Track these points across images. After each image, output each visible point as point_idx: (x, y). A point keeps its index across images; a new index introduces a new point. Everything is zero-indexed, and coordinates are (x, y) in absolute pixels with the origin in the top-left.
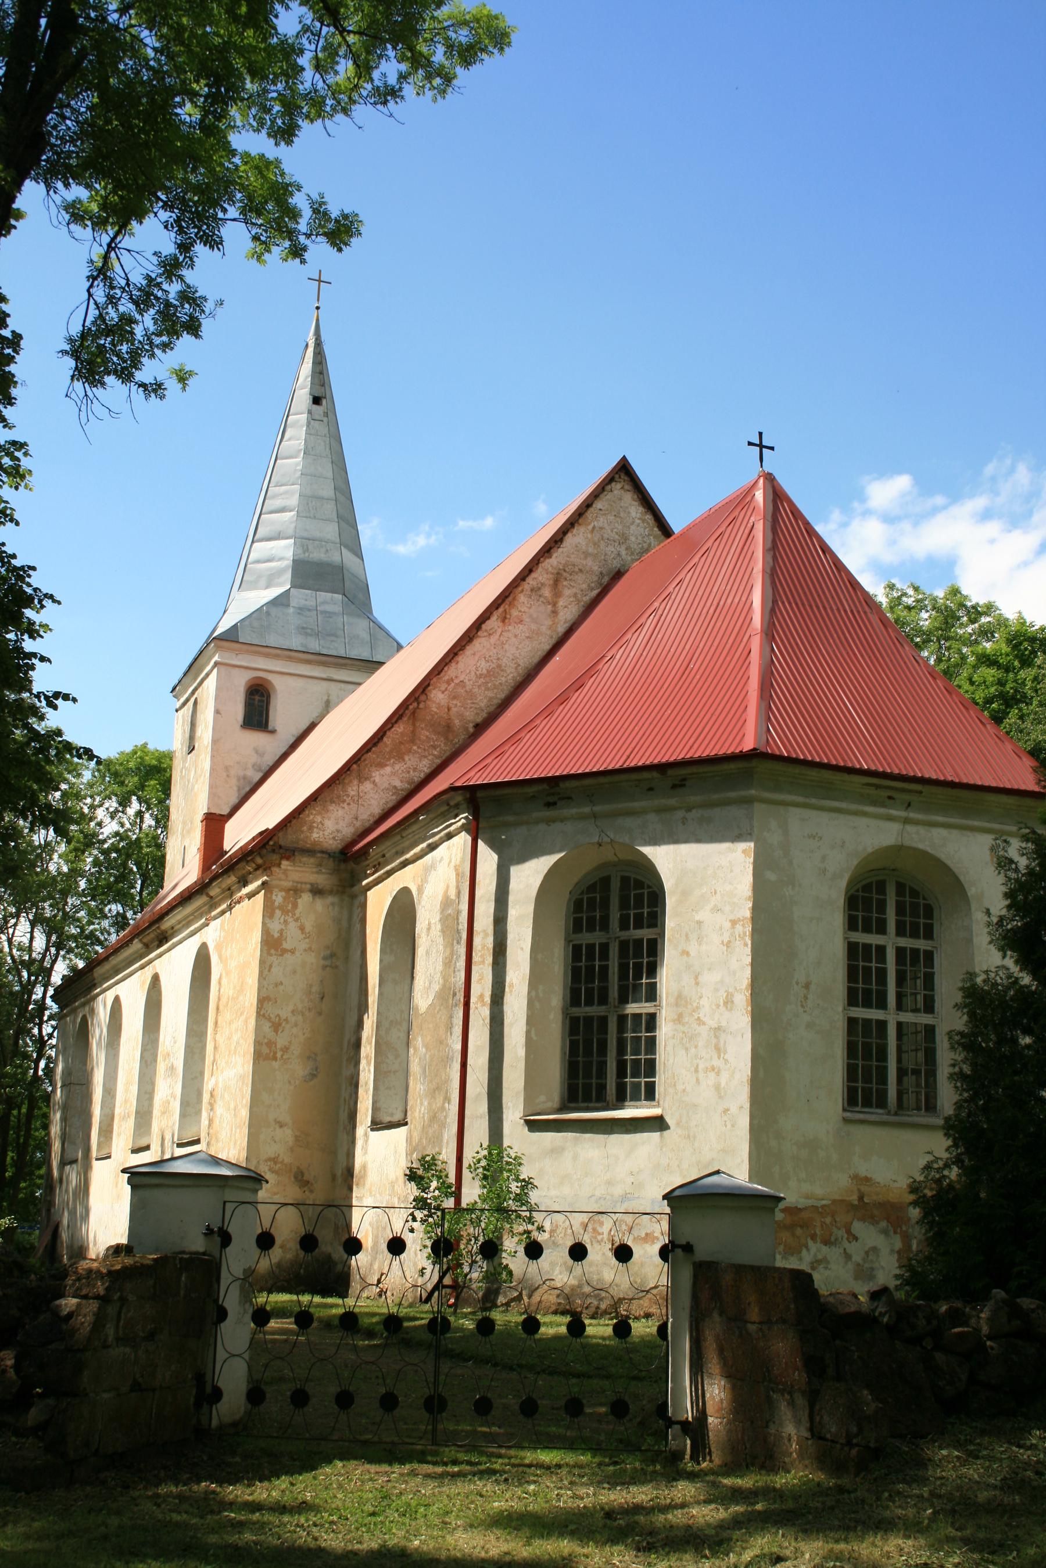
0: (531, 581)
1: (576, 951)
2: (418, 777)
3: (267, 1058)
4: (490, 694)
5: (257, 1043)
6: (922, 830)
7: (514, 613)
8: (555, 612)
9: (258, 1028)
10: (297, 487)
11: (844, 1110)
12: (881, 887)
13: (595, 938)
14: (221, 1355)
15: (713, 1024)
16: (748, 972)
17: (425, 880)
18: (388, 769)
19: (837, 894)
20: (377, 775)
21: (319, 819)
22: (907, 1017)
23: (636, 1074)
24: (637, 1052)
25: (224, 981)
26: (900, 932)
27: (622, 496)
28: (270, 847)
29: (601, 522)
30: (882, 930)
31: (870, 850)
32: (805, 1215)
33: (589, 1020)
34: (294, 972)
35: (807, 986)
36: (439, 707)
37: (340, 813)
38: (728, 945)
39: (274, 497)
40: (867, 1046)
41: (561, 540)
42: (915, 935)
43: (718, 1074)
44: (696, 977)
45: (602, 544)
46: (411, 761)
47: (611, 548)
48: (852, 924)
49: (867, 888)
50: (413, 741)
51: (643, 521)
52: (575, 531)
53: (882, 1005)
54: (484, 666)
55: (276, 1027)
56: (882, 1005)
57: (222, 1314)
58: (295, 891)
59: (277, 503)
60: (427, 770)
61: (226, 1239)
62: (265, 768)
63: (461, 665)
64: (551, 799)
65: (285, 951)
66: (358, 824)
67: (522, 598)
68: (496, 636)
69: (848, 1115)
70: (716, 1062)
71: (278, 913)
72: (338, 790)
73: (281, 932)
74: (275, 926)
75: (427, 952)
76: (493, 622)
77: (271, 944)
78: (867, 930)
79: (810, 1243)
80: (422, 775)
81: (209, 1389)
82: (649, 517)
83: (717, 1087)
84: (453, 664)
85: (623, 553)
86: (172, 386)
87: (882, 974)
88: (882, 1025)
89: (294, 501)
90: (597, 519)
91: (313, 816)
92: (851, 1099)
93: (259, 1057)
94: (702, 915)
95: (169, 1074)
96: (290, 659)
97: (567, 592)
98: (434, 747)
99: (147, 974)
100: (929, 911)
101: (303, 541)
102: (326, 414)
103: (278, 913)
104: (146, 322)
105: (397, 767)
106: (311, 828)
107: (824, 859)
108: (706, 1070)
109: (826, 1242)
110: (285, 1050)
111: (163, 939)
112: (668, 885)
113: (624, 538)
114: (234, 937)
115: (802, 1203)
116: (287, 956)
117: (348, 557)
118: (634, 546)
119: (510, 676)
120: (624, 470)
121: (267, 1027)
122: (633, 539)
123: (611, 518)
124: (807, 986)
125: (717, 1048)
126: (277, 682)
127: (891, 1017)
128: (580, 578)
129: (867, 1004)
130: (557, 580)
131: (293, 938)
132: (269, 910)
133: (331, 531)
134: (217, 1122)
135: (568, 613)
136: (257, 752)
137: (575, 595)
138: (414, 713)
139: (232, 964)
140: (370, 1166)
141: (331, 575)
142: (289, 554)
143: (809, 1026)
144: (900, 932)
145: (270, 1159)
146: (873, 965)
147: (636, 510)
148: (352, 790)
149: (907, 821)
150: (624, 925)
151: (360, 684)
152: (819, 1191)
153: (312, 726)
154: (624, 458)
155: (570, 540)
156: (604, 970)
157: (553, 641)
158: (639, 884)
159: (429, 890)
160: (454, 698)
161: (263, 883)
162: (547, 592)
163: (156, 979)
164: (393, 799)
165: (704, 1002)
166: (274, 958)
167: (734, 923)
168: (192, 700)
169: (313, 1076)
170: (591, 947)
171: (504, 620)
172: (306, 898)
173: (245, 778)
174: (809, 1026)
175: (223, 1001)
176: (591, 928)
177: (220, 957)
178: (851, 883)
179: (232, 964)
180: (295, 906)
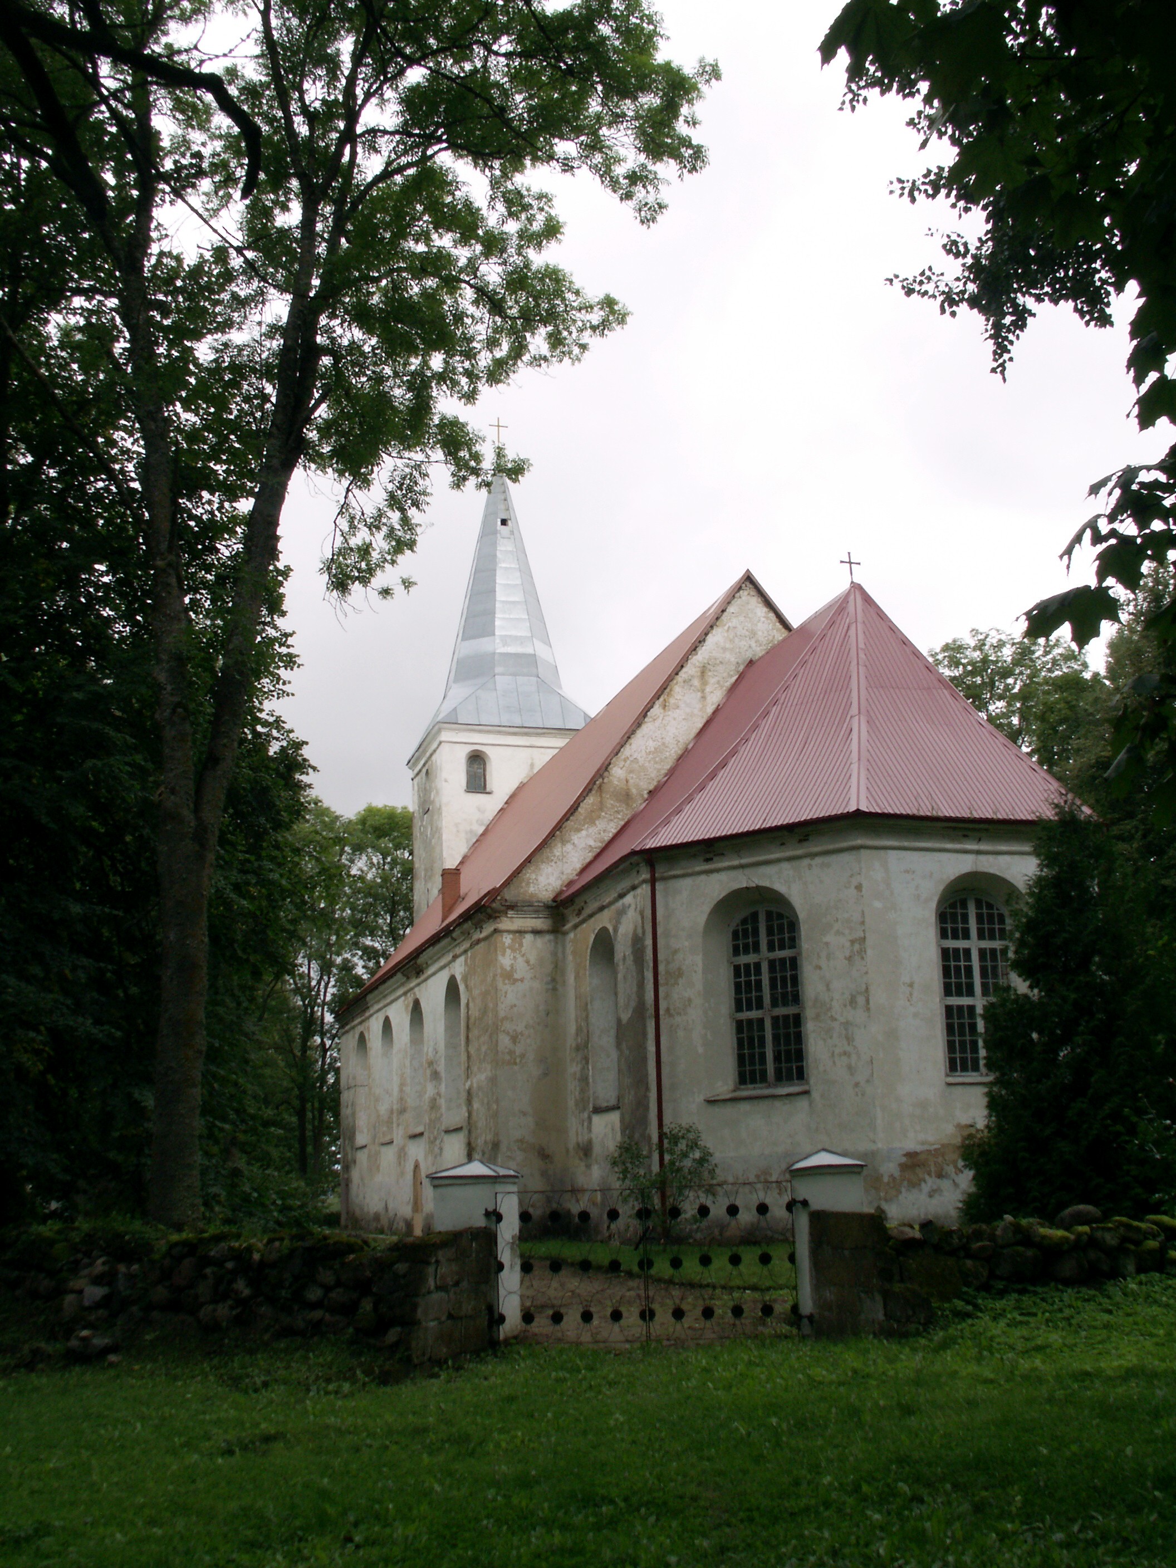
0: (683, 674)
1: (737, 969)
2: (608, 836)
4: (657, 766)
6: (991, 858)
7: (672, 701)
8: (704, 698)
11: (947, 1075)
13: (750, 958)
14: (502, 1292)
15: (842, 1020)
18: (584, 833)
19: (929, 913)
20: (575, 838)
21: (533, 876)
23: (788, 1060)
25: (471, 1005)
26: (981, 936)
27: (748, 599)
29: (734, 622)
30: (966, 936)
31: (952, 878)
32: (922, 1157)
33: (750, 1022)
34: (525, 996)
35: (911, 985)
36: (619, 780)
37: (550, 869)
40: (961, 1026)
44: (828, 986)
45: (737, 640)
46: (601, 824)
47: (743, 643)
48: (943, 934)
49: (953, 906)
50: (601, 809)
51: (767, 618)
52: (714, 631)
54: (651, 745)
56: (971, 993)
57: (501, 1267)
60: (614, 831)
61: (499, 1218)
63: (634, 746)
64: (708, 856)
65: (516, 980)
66: (564, 877)
68: (659, 721)
69: (950, 1080)
71: (508, 951)
72: (546, 852)
73: (512, 966)
75: (625, 978)
76: (656, 710)
78: (955, 937)
79: (927, 1177)
80: (611, 835)
81: (496, 1316)
82: (772, 615)
83: (849, 1067)
84: (627, 746)
85: (753, 645)
86: (399, 590)
87: (969, 970)
91: (529, 874)
92: (952, 1066)
94: (829, 938)
96: (499, 733)
97: (712, 681)
98: (618, 812)
99: (410, 999)
102: (512, 532)
104: (380, 542)
105: (590, 830)
106: (528, 884)
107: (917, 887)
108: (840, 1055)
109: (940, 1176)
110: (523, 1056)
111: (419, 971)
113: (753, 634)
115: (919, 1148)
116: (519, 983)
118: (761, 639)
120: (749, 579)
122: (760, 633)
123: (742, 619)
128: (721, 668)
129: (959, 994)
130: (703, 671)
134: (474, 1114)
136: (479, 810)
137: (718, 682)
138: (600, 787)
139: (476, 992)
140: (594, 1140)
143: (916, 1015)
144: (981, 936)
145: (517, 1141)
146: (962, 963)
147: (761, 610)
148: (557, 850)
149: (978, 852)
150: (771, 948)
152: (931, 1139)
155: (710, 639)
156: (759, 983)
157: (704, 721)
158: (780, 916)
159: (622, 930)
160: (631, 772)
162: (696, 682)
163: (417, 1004)
164: (590, 856)
165: (835, 1003)
166: (507, 987)
168: (424, 771)
169: (546, 1074)
170: (747, 966)
171: (664, 707)
173: (471, 831)
174: (916, 1015)
175: (472, 1020)
176: (746, 951)
177: (467, 986)
178: (940, 902)
179: (476, 992)
180: (521, 945)
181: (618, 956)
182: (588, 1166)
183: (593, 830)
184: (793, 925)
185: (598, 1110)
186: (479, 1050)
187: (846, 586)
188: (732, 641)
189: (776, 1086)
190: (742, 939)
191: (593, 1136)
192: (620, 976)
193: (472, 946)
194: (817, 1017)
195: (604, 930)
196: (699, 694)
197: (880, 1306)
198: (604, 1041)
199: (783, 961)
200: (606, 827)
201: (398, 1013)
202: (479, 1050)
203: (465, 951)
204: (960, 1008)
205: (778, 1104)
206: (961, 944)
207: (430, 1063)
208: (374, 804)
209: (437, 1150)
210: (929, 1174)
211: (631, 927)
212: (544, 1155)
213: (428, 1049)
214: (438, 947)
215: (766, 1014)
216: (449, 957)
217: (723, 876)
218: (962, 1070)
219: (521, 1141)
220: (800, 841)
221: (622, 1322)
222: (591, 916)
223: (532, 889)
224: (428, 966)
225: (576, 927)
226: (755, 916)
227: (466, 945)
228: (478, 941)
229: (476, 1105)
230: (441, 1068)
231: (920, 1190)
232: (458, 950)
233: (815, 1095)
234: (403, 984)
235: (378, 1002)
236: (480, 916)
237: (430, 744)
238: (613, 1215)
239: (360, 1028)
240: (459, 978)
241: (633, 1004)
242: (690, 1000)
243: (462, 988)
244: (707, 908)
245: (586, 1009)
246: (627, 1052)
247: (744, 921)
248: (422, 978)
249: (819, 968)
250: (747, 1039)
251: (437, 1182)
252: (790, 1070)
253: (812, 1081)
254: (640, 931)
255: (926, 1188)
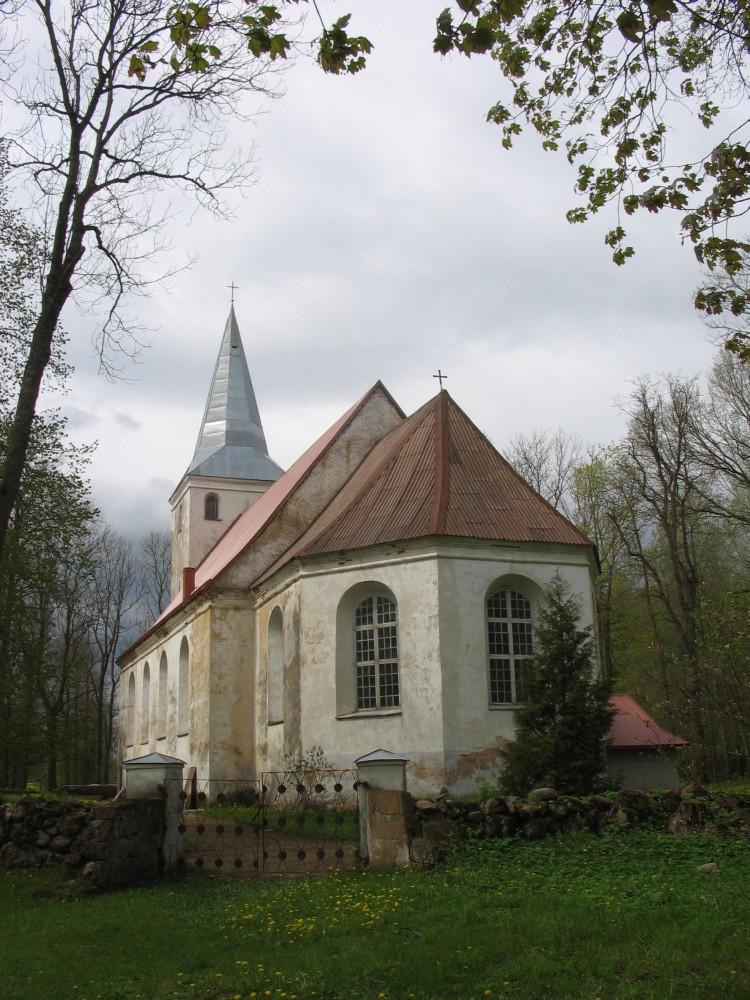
2: (283, 549)
3: (215, 693)
4: (318, 504)
5: (211, 686)
6: (521, 566)
7: (328, 463)
8: (348, 461)
9: (211, 678)
10: (226, 394)
12: (503, 595)
15: (422, 667)
16: (438, 642)
17: (286, 603)
18: (269, 546)
19: (481, 601)
20: (264, 549)
21: (235, 573)
22: (520, 657)
24: (389, 682)
27: (378, 398)
28: (213, 588)
29: (370, 413)
30: (505, 615)
31: (496, 577)
38: (428, 628)
39: (216, 399)
41: (349, 425)
42: (521, 617)
43: (427, 691)
46: (280, 540)
48: (490, 614)
49: (497, 595)
52: (356, 420)
53: (506, 651)
54: (314, 491)
55: (220, 677)
58: (226, 609)
59: (217, 402)
62: (218, 539)
67: (332, 455)
69: (493, 707)
70: (426, 686)
74: (217, 627)
76: (318, 469)
77: (215, 636)
79: (475, 770)
82: (393, 410)
83: (427, 698)
85: (381, 428)
87: (506, 637)
88: (507, 661)
89: (225, 401)
90: (368, 412)
91: (233, 572)
92: (494, 698)
93: (212, 692)
95: (162, 712)
96: (227, 482)
98: (291, 533)
99: (160, 650)
100: (528, 605)
101: (231, 422)
103: (218, 621)
109: (482, 768)
110: (225, 688)
111: (166, 633)
112: (399, 601)
114: (195, 630)
117: (254, 427)
119: (327, 495)
121: (216, 678)
124: (468, 646)
125: (426, 679)
126: (220, 493)
127: (512, 657)
130: (349, 445)
131: (226, 632)
132: (213, 620)
133: (245, 415)
135: (355, 461)
138: (280, 516)
139: (198, 646)
141: (246, 435)
142: (224, 428)
143: (470, 665)
147: (387, 406)
148: (251, 557)
149: (513, 562)
150: (380, 621)
151: (274, 482)
153: (241, 515)
154: (379, 381)
155: (353, 423)
158: (386, 600)
159: (288, 607)
161: (210, 607)
162: (344, 451)
163: (164, 653)
165: (419, 657)
167: (430, 618)
172: (232, 612)
178: (487, 594)
179: (198, 646)
180: (226, 616)
181: (285, 625)
182: (265, 760)
183: (274, 544)
184: (394, 606)
185: (271, 724)
186: (198, 684)
187: (439, 391)
188: (368, 425)
189: (381, 709)
190: (363, 615)
191: (268, 740)
192: (286, 638)
193: (195, 618)
194: (407, 666)
195: (277, 607)
196: (345, 459)
197: (407, 852)
198: (278, 679)
199: (387, 629)
200: (283, 541)
201: (153, 659)
202: (198, 684)
203: (192, 620)
204: (500, 661)
205: (381, 720)
206: (501, 620)
207: (171, 692)
208: (203, 514)
209: (173, 748)
210: (477, 767)
211: (293, 608)
212: (237, 751)
213: (170, 683)
214: (176, 618)
215: (376, 663)
216: (183, 624)
217: (350, 574)
218: (366, 707)
219: (223, 743)
220: (400, 552)
221: (235, 859)
222: (270, 599)
223: (234, 581)
224: (171, 630)
225: (261, 605)
226: (370, 600)
227: (193, 616)
228: (200, 614)
229: (196, 719)
230: (177, 695)
231: (471, 778)
232: (188, 620)
233: (405, 715)
234: (156, 642)
235: (142, 653)
236: (201, 598)
237: (183, 489)
238: (282, 789)
239: (131, 670)
240: (188, 637)
241: (293, 656)
242: (328, 654)
243: (190, 644)
244: (340, 595)
245: (266, 659)
246: (288, 687)
247: (364, 604)
248: (168, 637)
249: (410, 634)
250: (364, 679)
251: (129, 767)
252: (390, 699)
253: (403, 706)
254: (298, 608)
255: (474, 776)
